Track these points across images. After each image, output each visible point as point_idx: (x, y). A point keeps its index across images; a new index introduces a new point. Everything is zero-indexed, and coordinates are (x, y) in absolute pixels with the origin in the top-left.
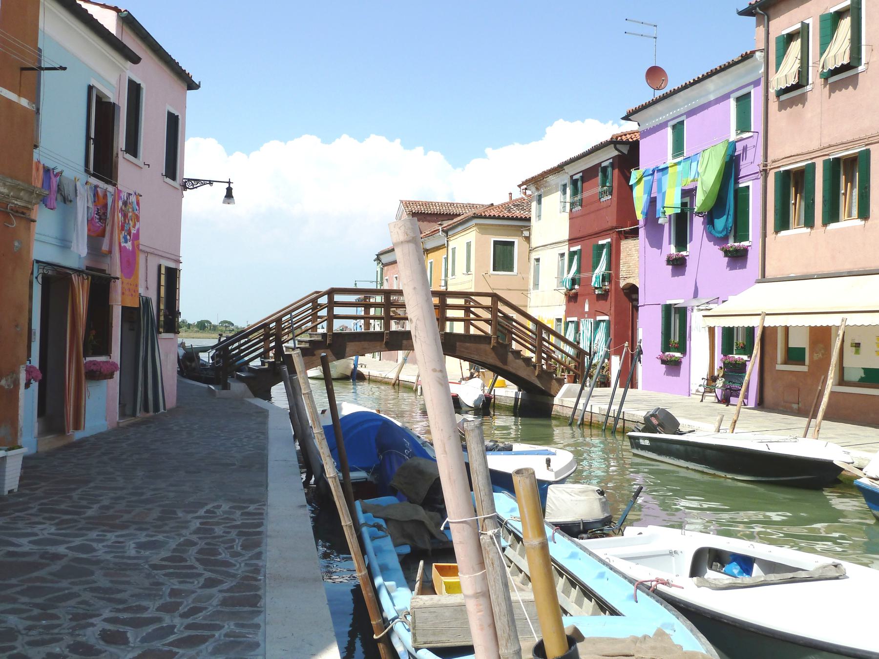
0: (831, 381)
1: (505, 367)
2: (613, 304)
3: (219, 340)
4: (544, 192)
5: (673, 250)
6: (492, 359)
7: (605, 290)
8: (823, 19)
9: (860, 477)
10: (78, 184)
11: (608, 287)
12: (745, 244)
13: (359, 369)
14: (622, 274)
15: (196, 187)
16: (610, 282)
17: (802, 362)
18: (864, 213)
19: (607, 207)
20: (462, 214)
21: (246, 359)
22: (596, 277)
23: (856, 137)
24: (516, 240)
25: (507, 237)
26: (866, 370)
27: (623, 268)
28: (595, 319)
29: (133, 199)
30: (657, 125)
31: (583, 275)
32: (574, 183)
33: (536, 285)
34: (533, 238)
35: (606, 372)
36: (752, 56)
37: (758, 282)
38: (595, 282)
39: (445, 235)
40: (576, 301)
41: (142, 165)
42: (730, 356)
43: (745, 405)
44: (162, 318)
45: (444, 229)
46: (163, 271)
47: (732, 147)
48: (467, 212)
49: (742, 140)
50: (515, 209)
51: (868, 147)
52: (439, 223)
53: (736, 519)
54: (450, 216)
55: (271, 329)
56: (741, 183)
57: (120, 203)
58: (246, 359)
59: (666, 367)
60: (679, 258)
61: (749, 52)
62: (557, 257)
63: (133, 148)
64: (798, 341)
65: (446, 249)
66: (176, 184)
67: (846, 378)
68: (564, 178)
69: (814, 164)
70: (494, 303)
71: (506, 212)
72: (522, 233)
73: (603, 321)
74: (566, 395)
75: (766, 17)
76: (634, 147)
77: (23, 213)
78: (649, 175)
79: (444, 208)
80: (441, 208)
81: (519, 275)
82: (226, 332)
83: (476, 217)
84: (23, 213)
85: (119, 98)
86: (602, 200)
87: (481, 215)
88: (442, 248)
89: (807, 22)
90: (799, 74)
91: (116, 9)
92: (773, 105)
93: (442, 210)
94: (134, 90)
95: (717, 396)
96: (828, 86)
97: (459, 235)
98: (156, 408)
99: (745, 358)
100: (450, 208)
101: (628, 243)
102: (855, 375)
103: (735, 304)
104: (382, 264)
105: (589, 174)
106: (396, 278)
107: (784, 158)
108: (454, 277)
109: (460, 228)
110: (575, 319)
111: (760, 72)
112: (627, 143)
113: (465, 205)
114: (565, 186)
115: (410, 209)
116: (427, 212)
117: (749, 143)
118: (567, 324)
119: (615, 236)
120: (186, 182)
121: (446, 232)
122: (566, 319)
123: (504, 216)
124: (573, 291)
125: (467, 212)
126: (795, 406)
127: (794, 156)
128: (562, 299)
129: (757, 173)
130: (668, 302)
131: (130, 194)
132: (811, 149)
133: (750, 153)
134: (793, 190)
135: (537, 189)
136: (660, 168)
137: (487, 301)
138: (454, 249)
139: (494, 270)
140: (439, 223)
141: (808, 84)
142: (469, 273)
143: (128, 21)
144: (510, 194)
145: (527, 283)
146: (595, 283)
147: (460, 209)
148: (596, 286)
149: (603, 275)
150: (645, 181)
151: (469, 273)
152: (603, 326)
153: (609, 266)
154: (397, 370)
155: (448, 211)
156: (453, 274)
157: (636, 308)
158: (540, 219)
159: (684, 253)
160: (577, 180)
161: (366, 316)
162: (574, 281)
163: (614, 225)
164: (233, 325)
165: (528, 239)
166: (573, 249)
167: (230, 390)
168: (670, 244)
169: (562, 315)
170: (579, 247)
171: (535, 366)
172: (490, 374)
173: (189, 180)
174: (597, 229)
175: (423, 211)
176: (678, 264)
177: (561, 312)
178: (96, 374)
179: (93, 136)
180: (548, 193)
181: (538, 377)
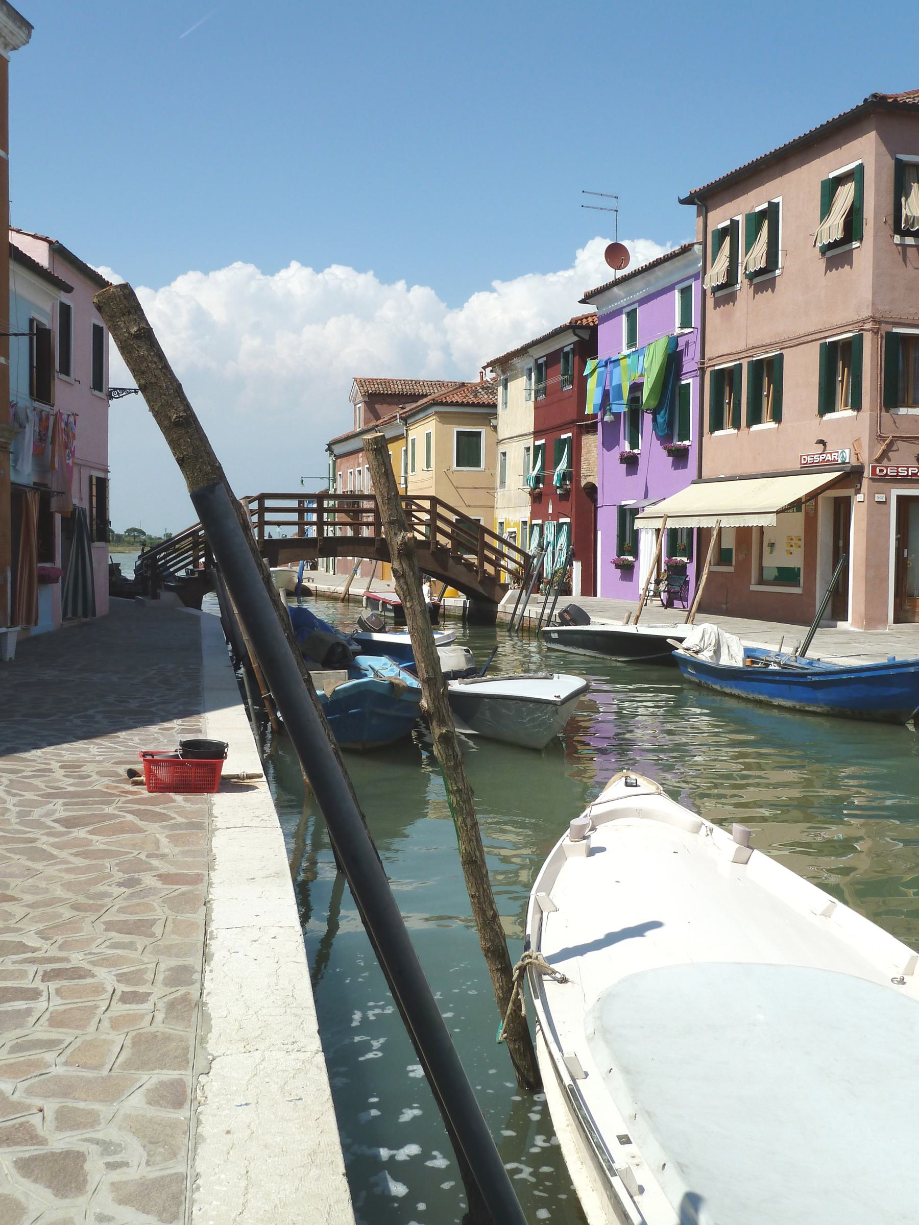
0: (706, 576)
1: (446, 574)
2: (574, 503)
3: (143, 550)
4: (510, 376)
5: (627, 448)
6: (432, 566)
7: (566, 490)
8: (749, 217)
9: (677, 649)
10: (28, 411)
11: (568, 487)
12: (686, 443)
13: (305, 583)
14: (583, 472)
15: (122, 397)
16: (571, 480)
17: (729, 563)
18: (777, 416)
19: (568, 398)
20: (430, 395)
21: (172, 570)
22: (558, 475)
23: (773, 341)
24: (483, 430)
25: (472, 427)
26: (780, 569)
27: (584, 465)
28: (558, 521)
29: (71, 419)
30: (613, 311)
31: (547, 473)
32: (539, 367)
33: (503, 482)
34: (500, 429)
35: (567, 579)
36: (690, 249)
37: (694, 482)
38: (555, 481)
39: (404, 422)
40: (540, 502)
41: (73, 382)
42: (674, 558)
43: (684, 607)
44: (94, 527)
45: (403, 416)
46: (94, 482)
47: (675, 341)
48: (436, 391)
49: (683, 335)
50: (483, 393)
51: (781, 352)
52: (401, 406)
53: (708, 736)
54: (415, 397)
55: (200, 537)
56: (683, 380)
57: (63, 425)
58: (172, 570)
59: (621, 572)
60: (631, 457)
61: (687, 245)
62: (522, 451)
63: (66, 369)
64: (729, 543)
65: (405, 439)
66: (102, 395)
67: (765, 577)
68: (527, 362)
69: (741, 365)
70: (433, 506)
71: (471, 397)
72: (490, 422)
73: (565, 523)
74: (508, 602)
75: (704, 208)
76: (594, 330)
77: (6, 448)
78: (602, 366)
79: (408, 387)
80: (404, 387)
81: (487, 471)
82: (135, 544)
83: (435, 403)
84: (6, 448)
85: (52, 324)
86: (565, 389)
87: (442, 401)
88: (401, 439)
89: (736, 218)
90: (727, 273)
91: (45, 239)
92: (710, 302)
93: (405, 390)
94: (65, 311)
95: (662, 600)
96: (753, 286)
97: (418, 424)
98: (94, 614)
99: (685, 560)
100: (415, 387)
101: (588, 439)
102: (770, 575)
103: (671, 505)
104: (335, 456)
105: (553, 358)
106: (351, 473)
107: (717, 357)
108: (414, 473)
109: (421, 415)
110: (539, 522)
111: (699, 265)
112: (587, 327)
113: (433, 383)
114: (530, 370)
115: (365, 389)
116: (386, 392)
117: (691, 338)
118: (532, 527)
119: (575, 430)
120: (112, 391)
121: (405, 419)
122: (531, 522)
123: (468, 402)
124: (537, 490)
125: (436, 391)
126: (724, 606)
127: (720, 356)
128: (528, 499)
129: (696, 370)
130: (623, 503)
131: (69, 415)
132: (738, 350)
133: (691, 349)
134: (727, 389)
135: (504, 372)
136: (612, 360)
137: (427, 504)
138: (413, 440)
139: (458, 465)
140: (401, 406)
141: (737, 283)
142: (429, 469)
143: (58, 251)
144: (480, 373)
145: (494, 481)
146: (556, 482)
147: (427, 388)
148: (558, 485)
149: (564, 473)
150: (598, 372)
151: (429, 469)
152: (565, 528)
153: (570, 464)
154: (346, 583)
155: (412, 390)
156: (413, 470)
157: (596, 509)
158: (506, 407)
159: (636, 451)
160: (567, 353)
161: (301, 521)
162: (538, 479)
163: (575, 418)
164: (144, 533)
165: (495, 428)
166: (538, 443)
167: (160, 598)
168: (625, 439)
169: (527, 519)
170: (543, 441)
171: (477, 572)
172: (441, 584)
173: (115, 389)
174: (559, 422)
175: (382, 392)
176: (631, 462)
177: (525, 513)
178: (46, 579)
179: (35, 365)
180: (515, 377)
181: (480, 582)
